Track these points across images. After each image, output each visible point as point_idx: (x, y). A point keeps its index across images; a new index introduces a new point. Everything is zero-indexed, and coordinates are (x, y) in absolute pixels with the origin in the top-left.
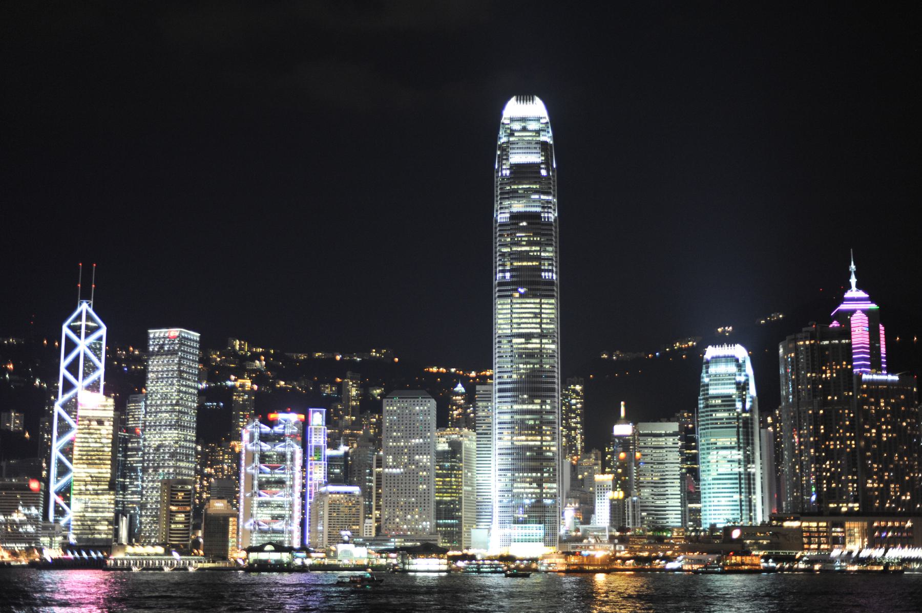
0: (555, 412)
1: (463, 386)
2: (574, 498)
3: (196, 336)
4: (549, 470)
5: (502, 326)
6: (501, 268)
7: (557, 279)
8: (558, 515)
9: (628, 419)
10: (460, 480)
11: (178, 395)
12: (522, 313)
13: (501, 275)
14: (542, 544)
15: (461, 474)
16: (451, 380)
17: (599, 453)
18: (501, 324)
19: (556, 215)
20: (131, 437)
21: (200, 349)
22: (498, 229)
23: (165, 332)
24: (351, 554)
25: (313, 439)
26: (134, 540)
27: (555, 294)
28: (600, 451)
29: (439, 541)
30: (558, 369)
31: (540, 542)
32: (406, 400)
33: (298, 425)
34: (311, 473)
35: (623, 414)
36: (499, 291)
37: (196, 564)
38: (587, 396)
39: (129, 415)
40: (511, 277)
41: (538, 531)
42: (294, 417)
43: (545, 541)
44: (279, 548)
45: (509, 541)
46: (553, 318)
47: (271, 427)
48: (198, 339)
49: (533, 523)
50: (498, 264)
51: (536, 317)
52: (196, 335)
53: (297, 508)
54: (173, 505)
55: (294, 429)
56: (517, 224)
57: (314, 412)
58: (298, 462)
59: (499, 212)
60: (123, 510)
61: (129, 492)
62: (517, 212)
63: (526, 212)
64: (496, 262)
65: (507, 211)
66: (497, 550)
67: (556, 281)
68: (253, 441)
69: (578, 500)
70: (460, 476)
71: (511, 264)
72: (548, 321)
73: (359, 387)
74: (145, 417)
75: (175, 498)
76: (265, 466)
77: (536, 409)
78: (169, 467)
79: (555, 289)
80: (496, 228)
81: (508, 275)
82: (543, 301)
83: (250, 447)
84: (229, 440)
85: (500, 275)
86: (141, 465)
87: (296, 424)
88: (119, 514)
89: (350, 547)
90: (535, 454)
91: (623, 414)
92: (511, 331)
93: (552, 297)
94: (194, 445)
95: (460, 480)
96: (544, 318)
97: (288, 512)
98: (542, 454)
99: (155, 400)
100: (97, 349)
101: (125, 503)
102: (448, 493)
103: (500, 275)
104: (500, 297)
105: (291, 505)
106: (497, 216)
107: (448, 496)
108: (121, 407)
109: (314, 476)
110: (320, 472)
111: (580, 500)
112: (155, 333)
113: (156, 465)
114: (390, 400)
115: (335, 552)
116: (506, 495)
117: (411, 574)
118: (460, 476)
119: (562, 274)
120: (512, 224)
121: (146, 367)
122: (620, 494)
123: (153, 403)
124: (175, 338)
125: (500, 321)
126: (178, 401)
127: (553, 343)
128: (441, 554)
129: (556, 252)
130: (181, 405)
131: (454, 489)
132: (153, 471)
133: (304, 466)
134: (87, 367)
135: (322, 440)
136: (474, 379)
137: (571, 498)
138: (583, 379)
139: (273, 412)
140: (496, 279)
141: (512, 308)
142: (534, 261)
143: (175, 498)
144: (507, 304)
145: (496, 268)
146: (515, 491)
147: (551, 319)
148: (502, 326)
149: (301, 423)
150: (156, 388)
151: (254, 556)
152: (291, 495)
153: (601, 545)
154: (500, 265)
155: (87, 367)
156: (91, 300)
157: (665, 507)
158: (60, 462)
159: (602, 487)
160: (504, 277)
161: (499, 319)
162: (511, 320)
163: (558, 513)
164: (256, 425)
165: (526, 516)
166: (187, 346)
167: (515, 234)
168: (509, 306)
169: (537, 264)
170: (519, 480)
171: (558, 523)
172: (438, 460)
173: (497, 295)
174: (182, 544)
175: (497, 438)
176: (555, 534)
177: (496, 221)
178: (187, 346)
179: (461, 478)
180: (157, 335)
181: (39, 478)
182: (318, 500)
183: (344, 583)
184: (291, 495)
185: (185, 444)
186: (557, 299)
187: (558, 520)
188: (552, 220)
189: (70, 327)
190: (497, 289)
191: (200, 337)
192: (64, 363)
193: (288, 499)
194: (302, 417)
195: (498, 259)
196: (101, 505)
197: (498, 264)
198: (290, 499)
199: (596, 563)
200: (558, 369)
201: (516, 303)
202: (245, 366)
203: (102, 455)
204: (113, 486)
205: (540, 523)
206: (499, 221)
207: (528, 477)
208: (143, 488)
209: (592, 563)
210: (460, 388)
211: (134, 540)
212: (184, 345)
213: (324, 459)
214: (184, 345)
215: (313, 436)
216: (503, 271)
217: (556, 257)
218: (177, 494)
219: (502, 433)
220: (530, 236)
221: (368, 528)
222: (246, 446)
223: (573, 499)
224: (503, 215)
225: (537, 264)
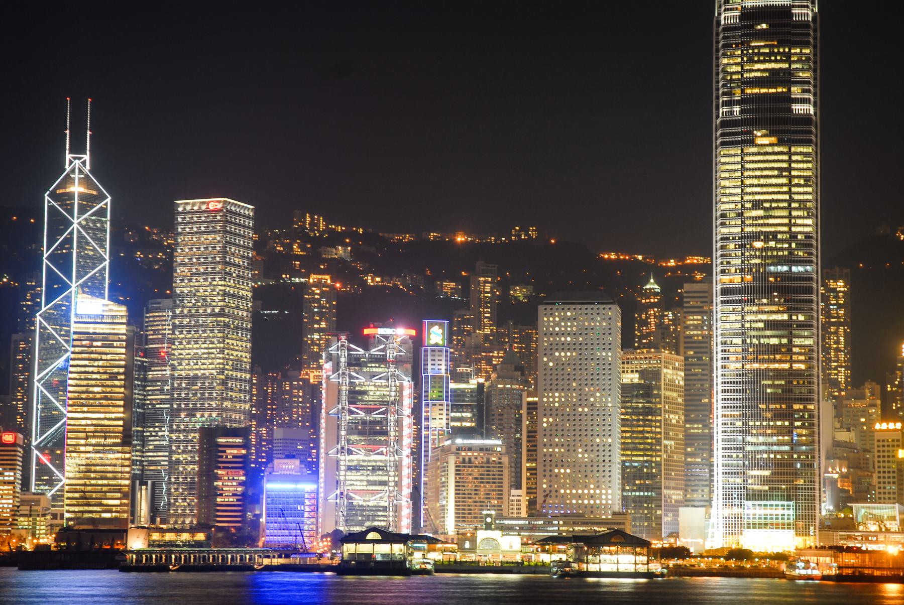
0: (812, 326)
1: (657, 282)
2: (839, 458)
4: (803, 416)
7: (815, 113)
8: (817, 487)
10: (658, 430)
11: (224, 300)
12: (759, 169)
13: (726, 109)
14: (792, 532)
15: (660, 421)
16: (638, 274)
17: (878, 388)
18: (726, 187)
19: (816, 10)
20: (152, 364)
21: (256, 229)
22: (721, 36)
23: (202, 203)
24: (498, 545)
25: (430, 367)
26: (158, 519)
27: (813, 138)
28: (878, 384)
29: (627, 524)
30: (817, 257)
31: (789, 528)
32: (574, 307)
33: (407, 345)
34: (427, 419)
36: (722, 135)
37: (260, 560)
38: (853, 299)
39: (147, 331)
40: (741, 112)
42: (401, 333)
43: (796, 528)
44: (388, 537)
45: (736, 525)
46: (810, 177)
47: (366, 348)
48: (251, 214)
49: (777, 498)
50: (720, 92)
51: (780, 176)
52: (248, 209)
53: (406, 471)
54: (219, 468)
55: (400, 351)
56: (752, 27)
57: (432, 325)
58: (408, 402)
59: (723, 8)
60: (142, 474)
61: (151, 447)
62: (753, 8)
64: (718, 90)
66: (717, 540)
67: (814, 118)
68: (338, 370)
69: (846, 462)
70: (658, 424)
71: (743, 91)
72: (802, 182)
73: (495, 285)
74: (174, 333)
75: (222, 457)
76: (357, 408)
77: (783, 321)
78: (212, 410)
79: (813, 129)
80: (718, 34)
81: (737, 109)
82: (793, 149)
83: (334, 378)
84: (299, 366)
85: (723, 110)
86: (168, 406)
87: (403, 342)
88: (139, 479)
89: (496, 534)
93: (807, 142)
94: (248, 376)
95: (658, 430)
96: (795, 177)
97: (391, 479)
98: (791, 391)
99: (187, 307)
100: (98, 229)
101: (145, 463)
102: (640, 450)
103: (723, 110)
104: (723, 144)
105: (398, 467)
106: (720, 14)
107: (640, 455)
108: (135, 317)
109: (433, 424)
110: (441, 417)
111: (849, 464)
112: (186, 204)
113: (191, 406)
114: (549, 307)
115: (473, 540)
116: (735, 455)
117: (591, 580)
118: (658, 424)
119: (824, 102)
120: (744, 27)
121: (171, 257)
123: (185, 311)
124: (216, 211)
125: (724, 183)
126: (222, 309)
128: (638, 547)
129: (815, 71)
130: (228, 316)
131: (648, 444)
132: (187, 416)
133: (416, 411)
134: (82, 257)
135: (443, 368)
136: (673, 269)
137: (833, 458)
138: (849, 271)
139: (368, 327)
140: (717, 117)
141: (743, 162)
142: (779, 86)
143: (222, 457)
144: (735, 155)
145: (718, 98)
146: (749, 448)
147: (807, 179)
149: (411, 341)
150: (189, 289)
151: (349, 548)
152: (397, 452)
153: (888, 535)
154: (724, 94)
155: (82, 257)
156: (86, 154)
158: (46, 403)
160: (732, 113)
161: (723, 179)
162: (742, 181)
163: (817, 484)
164: (343, 346)
165: (767, 488)
166: (235, 224)
167: (749, 42)
168: (738, 159)
169: (784, 90)
170: (754, 432)
171: (817, 498)
172: (623, 399)
173: (719, 141)
174: (234, 527)
175: (719, 367)
176: (814, 517)
177: (719, 23)
178: (235, 224)
179: (660, 427)
180: (188, 208)
181: (15, 429)
182: (438, 460)
184: (397, 452)
185: (234, 374)
186: (816, 146)
187: (817, 495)
188: (810, 19)
189: (53, 195)
190: (719, 132)
191: (254, 210)
193: (392, 459)
194: (413, 332)
195: (721, 84)
196: (110, 468)
197: (720, 92)
199: (885, 566)
200: (817, 257)
202: (320, 254)
203: (110, 393)
204: (126, 440)
205: (789, 499)
206: (723, 23)
207: (769, 427)
208: (171, 440)
209: (878, 565)
210: (652, 285)
211: (158, 519)
212: (231, 223)
213: (447, 397)
214: (231, 223)
216: (729, 103)
217: (815, 79)
218: (225, 452)
219: (728, 358)
220: (774, 46)
221: (515, 503)
222: (328, 378)
223: (837, 461)
224: (729, 14)
225: (784, 90)
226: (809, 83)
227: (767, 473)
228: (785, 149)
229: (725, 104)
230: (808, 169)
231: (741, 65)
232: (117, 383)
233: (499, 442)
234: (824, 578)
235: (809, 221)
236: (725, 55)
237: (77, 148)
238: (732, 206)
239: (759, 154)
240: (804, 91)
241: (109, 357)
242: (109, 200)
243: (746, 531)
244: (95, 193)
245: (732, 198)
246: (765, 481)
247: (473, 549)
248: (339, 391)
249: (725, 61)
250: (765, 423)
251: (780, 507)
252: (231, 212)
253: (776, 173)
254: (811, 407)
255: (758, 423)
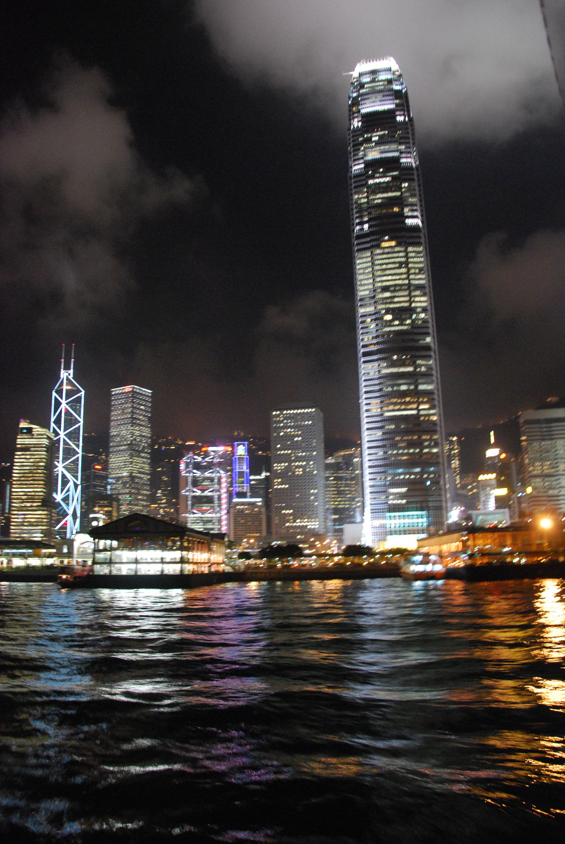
0: (432, 375)
3: (149, 393)
5: (363, 282)
6: (357, 221)
9: (495, 445)
13: (358, 228)
22: (353, 186)
25: (237, 467)
35: (492, 440)
41: (420, 520)
45: (385, 533)
57: (238, 445)
63: (381, 158)
65: (361, 161)
81: (366, 226)
90: (411, 426)
91: (492, 440)
92: (374, 285)
93: (418, 244)
104: (358, 250)
105: (220, 521)
122: (503, 492)
124: (129, 392)
127: (424, 295)
147: (421, 270)
148: (363, 282)
157: (559, 496)
159: (486, 485)
162: (373, 274)
165: (404, 501)
176: (442, 524)
183: (421, 579)
192: (53, 419)
198: (218, 515)
201: (378, 260)
215: (237, 464)
226: (416, 205)
227: (404, 490)
228: (402, 249)
229: (358, 224)
230: (420, 262)
231: (367, 197)
232: (39, 471)
233: (260, 499)
234: (450, 574)
235: (423, 299)
236: (356, 193)
237: (67, 368)
238: (367, 292)
239: (383, 254)
240: (413, 211)
241: (36, 456)
242: (83, 393)
243: (389, 537)
244: (75, 389)
245: (366, 287)
246: (402, 496)
247: (70, 554)
248: (187, 480)
249: (356, 197)
250: (401, 451)
251: (416, 517)
252: (136, 392)
253: (397, 265)
254: (435, 437)
255: (395, 452)
